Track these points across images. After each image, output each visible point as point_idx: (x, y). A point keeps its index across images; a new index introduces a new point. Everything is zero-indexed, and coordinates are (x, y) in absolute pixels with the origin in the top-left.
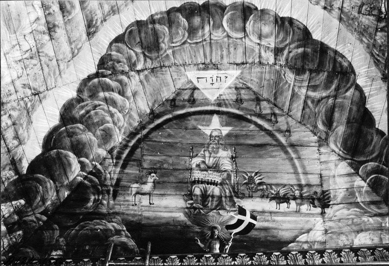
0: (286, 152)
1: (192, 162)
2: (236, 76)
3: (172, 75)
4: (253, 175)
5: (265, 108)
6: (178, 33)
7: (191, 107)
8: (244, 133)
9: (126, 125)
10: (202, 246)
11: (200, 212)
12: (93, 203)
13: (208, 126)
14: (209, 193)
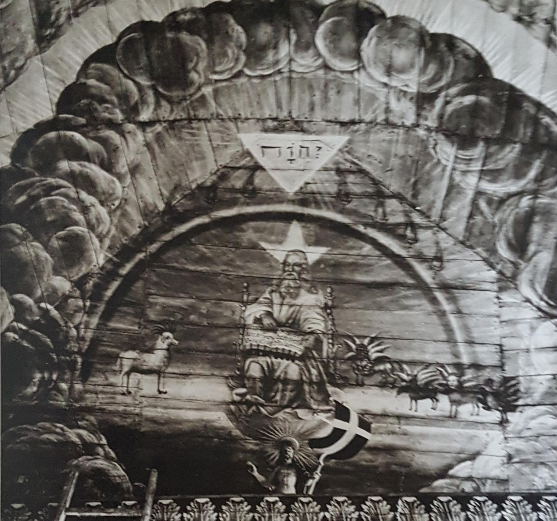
0: (434, 301)
1: (247, 313)
2: (339, 146)
3: (212, 138)
4: (366, 342)
5: (394, 213)
6: (225, 55)
7: (248, 204)
8: (350, 260)
9: (113, 231)
10: (261, 478)
11: (260, 412)
12: (39, 387)
13: (280, 243)
14: (277, 374)
